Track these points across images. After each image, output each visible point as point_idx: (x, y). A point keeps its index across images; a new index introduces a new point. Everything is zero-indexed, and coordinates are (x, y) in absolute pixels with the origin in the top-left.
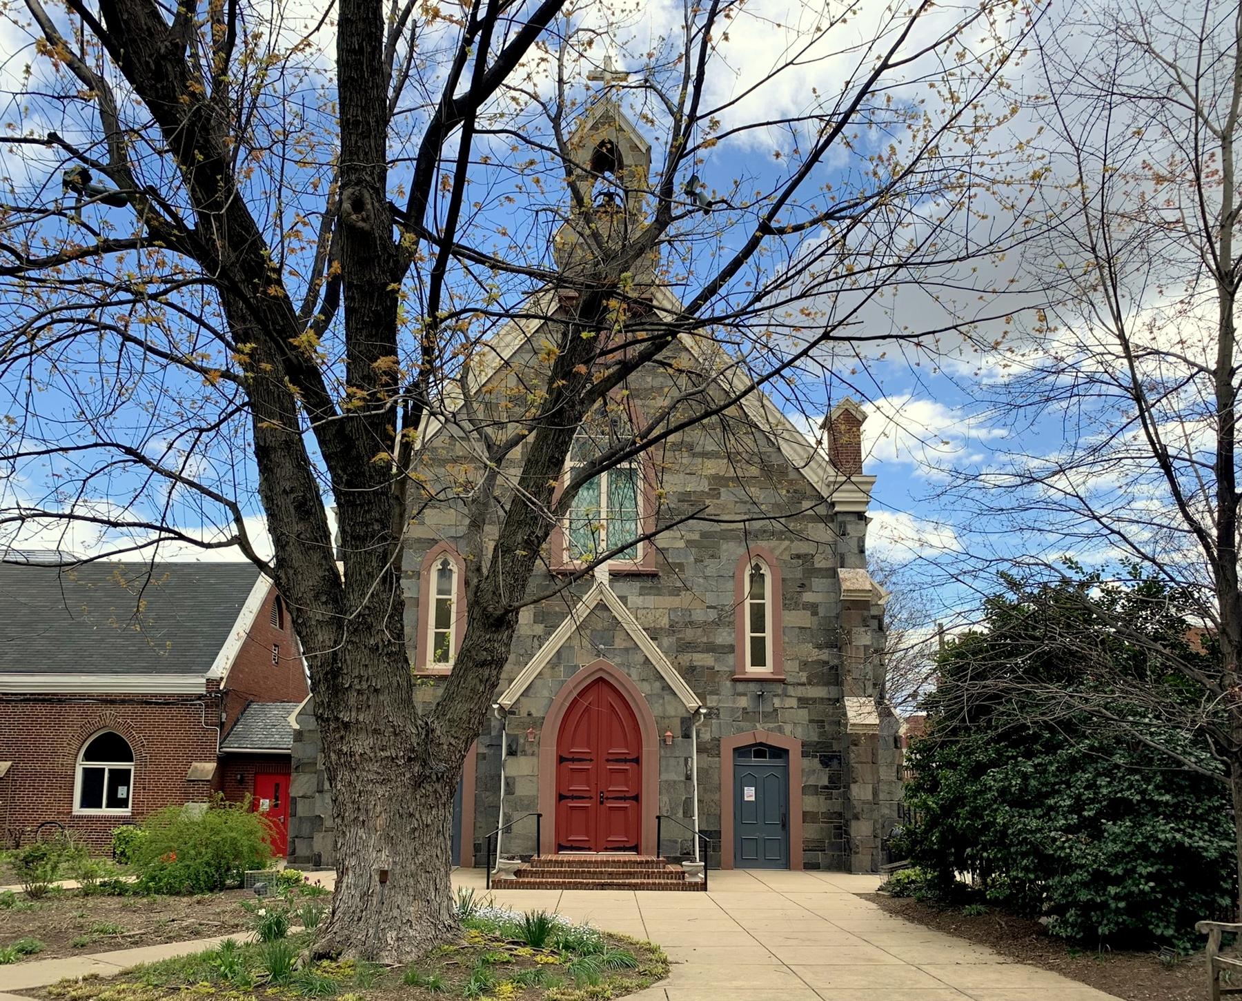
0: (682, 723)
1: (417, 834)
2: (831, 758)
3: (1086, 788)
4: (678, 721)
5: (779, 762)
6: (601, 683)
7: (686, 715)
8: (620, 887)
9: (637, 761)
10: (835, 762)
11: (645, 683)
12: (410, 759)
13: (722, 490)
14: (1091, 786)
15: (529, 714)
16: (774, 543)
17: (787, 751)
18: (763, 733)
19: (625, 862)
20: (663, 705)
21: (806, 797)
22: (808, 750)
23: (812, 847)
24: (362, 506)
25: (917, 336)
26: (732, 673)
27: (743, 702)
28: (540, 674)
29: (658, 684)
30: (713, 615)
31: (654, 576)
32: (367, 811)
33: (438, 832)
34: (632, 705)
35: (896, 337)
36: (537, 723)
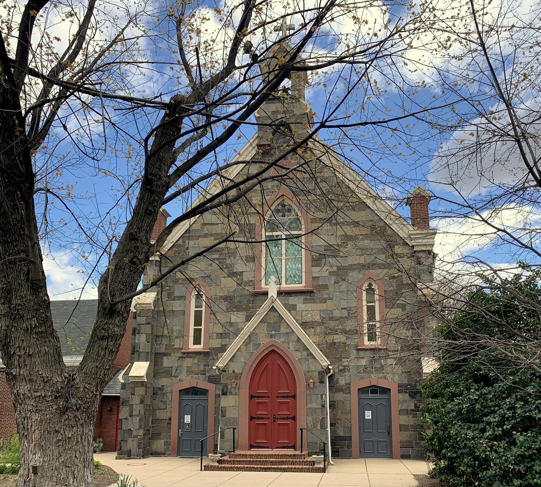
0: (319, 374)
1: (61, 443)
2: (415, 393)
3: (509, 409)
4: (317, 373)
5: (385, 396)
6: (273, 352)
7: (321, 370)
8: (276, 470)
9: (294, 397)
10: (418, 395)
11: (298, 352)
12: (56, 397)
13: (348, 242)
14: (512, 408)
15: (234, 372)
16: (379, 271)
17: (390, 389)
18: (374, 380)
19: (282, 455)
20: (308, 364)
21: (401, 417)
22: (402, 388)
23: (405, 445)
24: (12, 243)
25: (386, 122)
26: (357, 345)
27: (363, 362)
28: (239, 349)
29: (305, 353)
30: (345, 313)
31: (311, 292)
32: (28, 429)
33: (77, 442)
34: (291, 365)
35: (371, 123)
36: (237, 376)
